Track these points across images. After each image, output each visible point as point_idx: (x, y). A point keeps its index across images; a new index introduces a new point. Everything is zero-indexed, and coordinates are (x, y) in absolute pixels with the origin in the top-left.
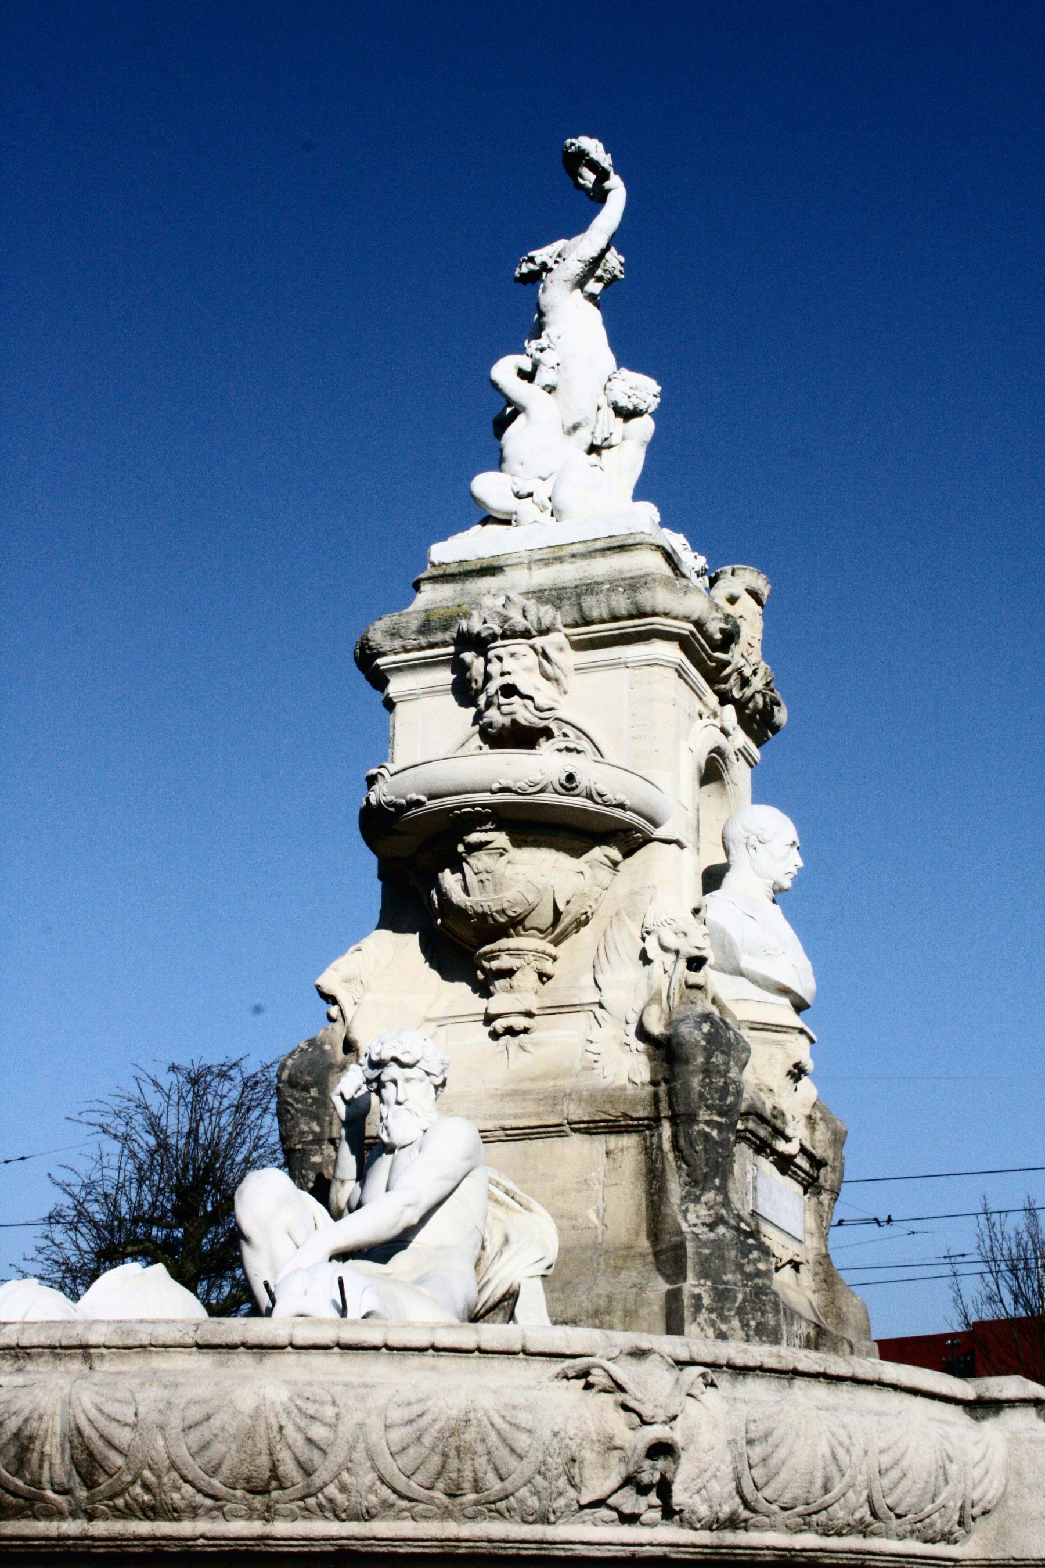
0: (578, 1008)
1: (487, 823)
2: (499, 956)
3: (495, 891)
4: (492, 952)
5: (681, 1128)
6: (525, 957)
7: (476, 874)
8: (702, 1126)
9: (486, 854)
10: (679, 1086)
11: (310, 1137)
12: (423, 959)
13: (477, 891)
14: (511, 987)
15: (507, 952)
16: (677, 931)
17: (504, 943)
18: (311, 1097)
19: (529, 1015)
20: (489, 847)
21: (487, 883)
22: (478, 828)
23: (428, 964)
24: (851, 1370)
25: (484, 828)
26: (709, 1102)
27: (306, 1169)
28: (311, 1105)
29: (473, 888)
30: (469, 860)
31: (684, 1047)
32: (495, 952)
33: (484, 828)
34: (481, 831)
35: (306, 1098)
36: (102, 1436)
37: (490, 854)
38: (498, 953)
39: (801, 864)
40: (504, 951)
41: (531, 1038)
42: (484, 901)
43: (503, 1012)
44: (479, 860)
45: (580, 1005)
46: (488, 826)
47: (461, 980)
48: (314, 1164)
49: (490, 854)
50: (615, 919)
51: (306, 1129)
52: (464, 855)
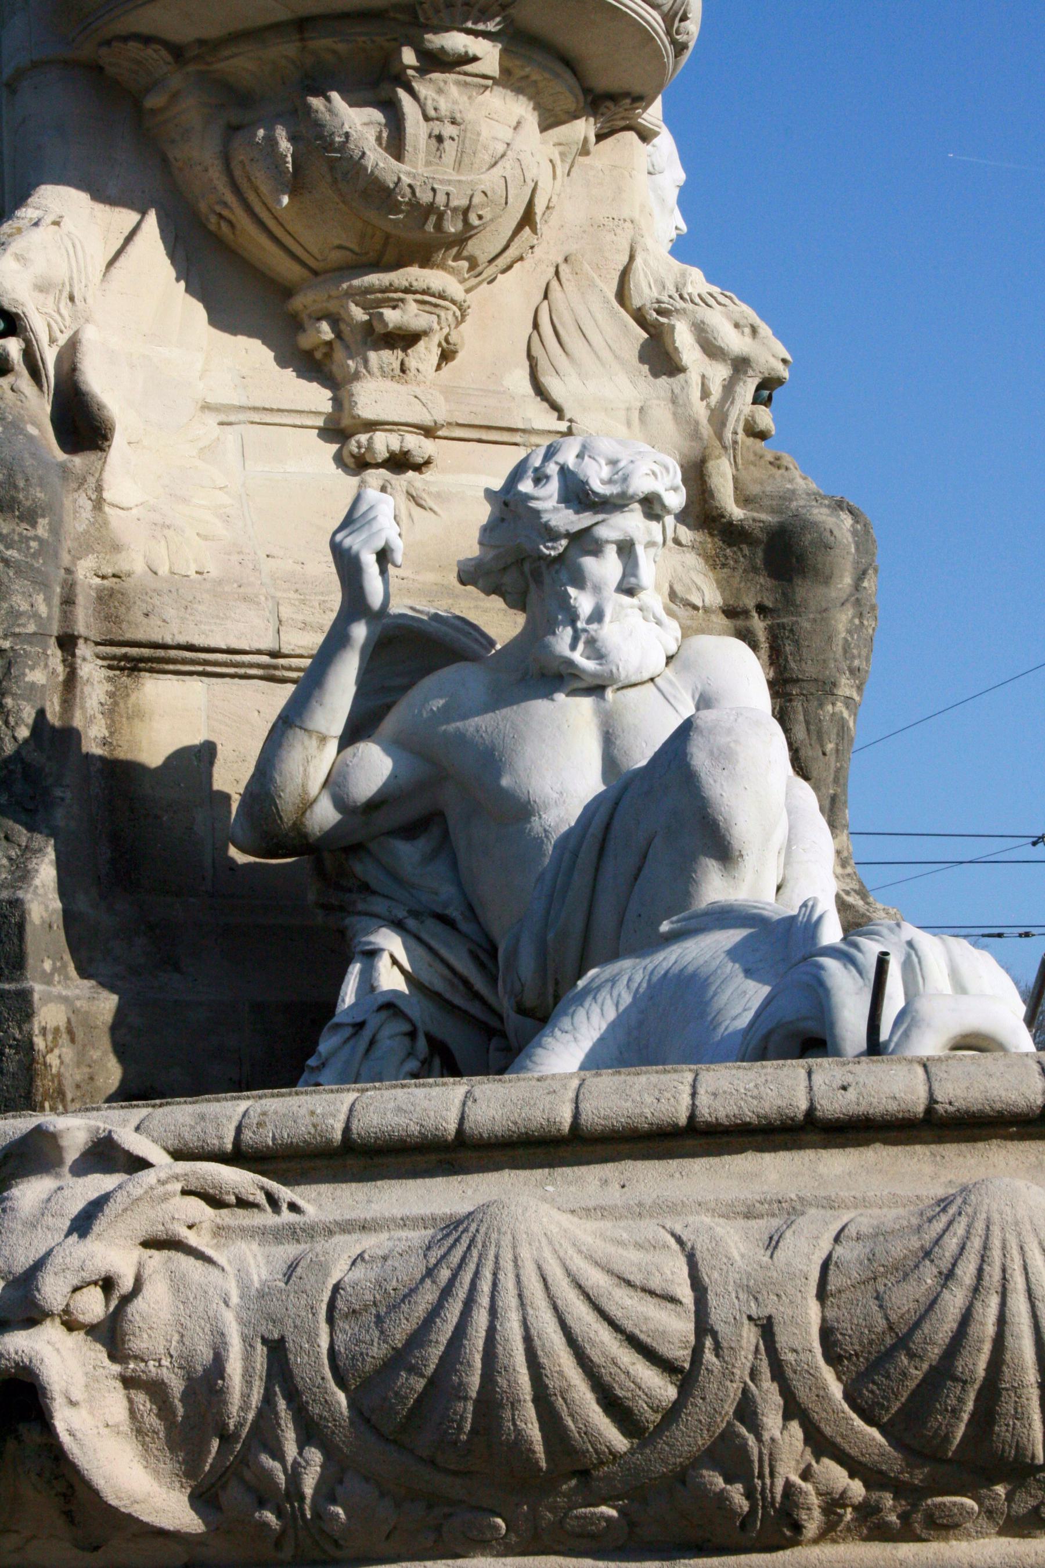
0: (517, 438)
1: (491, 18)
2: (402, 300)
3: (458, 165)
4: (390, 288)
5: (798, 705)
6: (442, 314)
7: (427, 118)
8: (840, 706)
9: (458, 83)
10: (807, 625)
11: (31, 628)
12: (172, 273)
13: (422, 156)
14: (403, 371)
15: (419, 297)
16: (742, 322)
17: (414, 275)
18: (36, 538)
19: (428, 432)
20: (468, 68)
21: (447, 143)
22: (469, 25)
23: (182, 284)
24: (822, 1169)
25: (481, 27)
26: (856, 663)
27: (14, 696)
28: (34, 556)
29: (415, 149)
30: (422, 88)
31: (832, 552)
32: (396, 291)
33: (481, 27)
34: (469, 32)
35: (28, 539)
36: (1004, 1270)
37: (466, 84)
38: (400, 295)
39: (684, 228)
40: (415, 292)
41: (427, 482)
42: (441, 182)
43: (390, 419)
44: (440, 91)
45: (524, 431)
46: (491, 26)
47: (251, 332)
48: (33, 686)
49: (466, 84)
50: (564, 269)
51: (24, 607)
52: (410, 72)
